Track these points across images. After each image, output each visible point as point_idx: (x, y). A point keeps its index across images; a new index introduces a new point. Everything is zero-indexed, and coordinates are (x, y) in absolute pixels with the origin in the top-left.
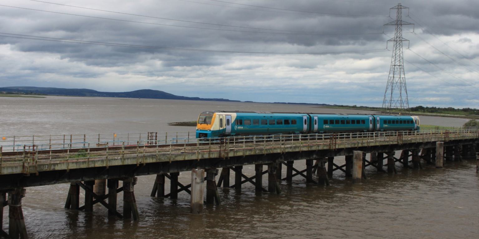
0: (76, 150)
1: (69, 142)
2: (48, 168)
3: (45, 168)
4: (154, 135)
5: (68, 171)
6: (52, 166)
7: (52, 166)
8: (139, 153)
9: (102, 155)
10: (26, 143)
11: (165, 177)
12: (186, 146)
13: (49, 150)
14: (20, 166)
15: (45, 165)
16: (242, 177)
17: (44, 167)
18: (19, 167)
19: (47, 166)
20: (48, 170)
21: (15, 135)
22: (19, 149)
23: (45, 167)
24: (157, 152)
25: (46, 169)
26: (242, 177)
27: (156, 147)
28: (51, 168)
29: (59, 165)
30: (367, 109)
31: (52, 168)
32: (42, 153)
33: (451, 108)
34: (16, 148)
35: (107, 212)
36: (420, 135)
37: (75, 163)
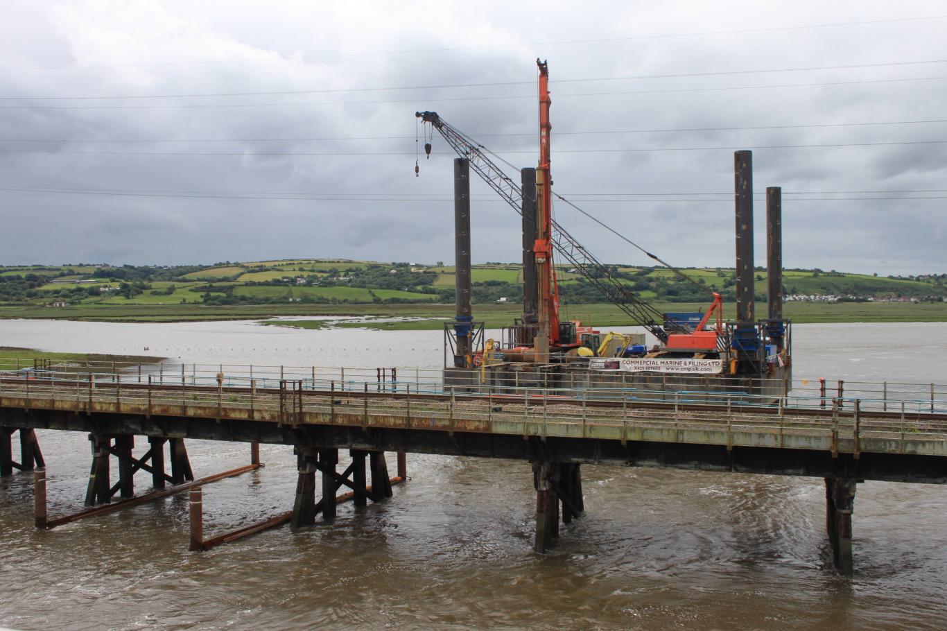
0: (938, 417)
1: (835, 394)
2: (896, 447)
3: (890, 447)
4: (389, 372)
5: (729, 449)
6: (909, 445)
7: (909, 445)
8: (547, 414)
9: (755, 423)
10: (408, 380)
11: (151, 458)
12: (627, 407)
13: (900, 411)
14: (827, 437)
15: (889, 441)
16: (13, 468)
17: (888, 444)
18: (823, 440)
19: (894, 444)
20: (898, 452)
21: (196, 363)
22: (922, 408)
23: (890, 444)
24: (526, 413)
25: (891, 449)
26: (13, 468)
27: (623, 407)
28: (905, 448)
29: (927, 445)
30: (875, 303)
31: (909, 449)
32: (230, 391)
33: (817, 272)
34: (346, 387)
35: (62, 514)
36: (526, 406)
37: (701, 433)
